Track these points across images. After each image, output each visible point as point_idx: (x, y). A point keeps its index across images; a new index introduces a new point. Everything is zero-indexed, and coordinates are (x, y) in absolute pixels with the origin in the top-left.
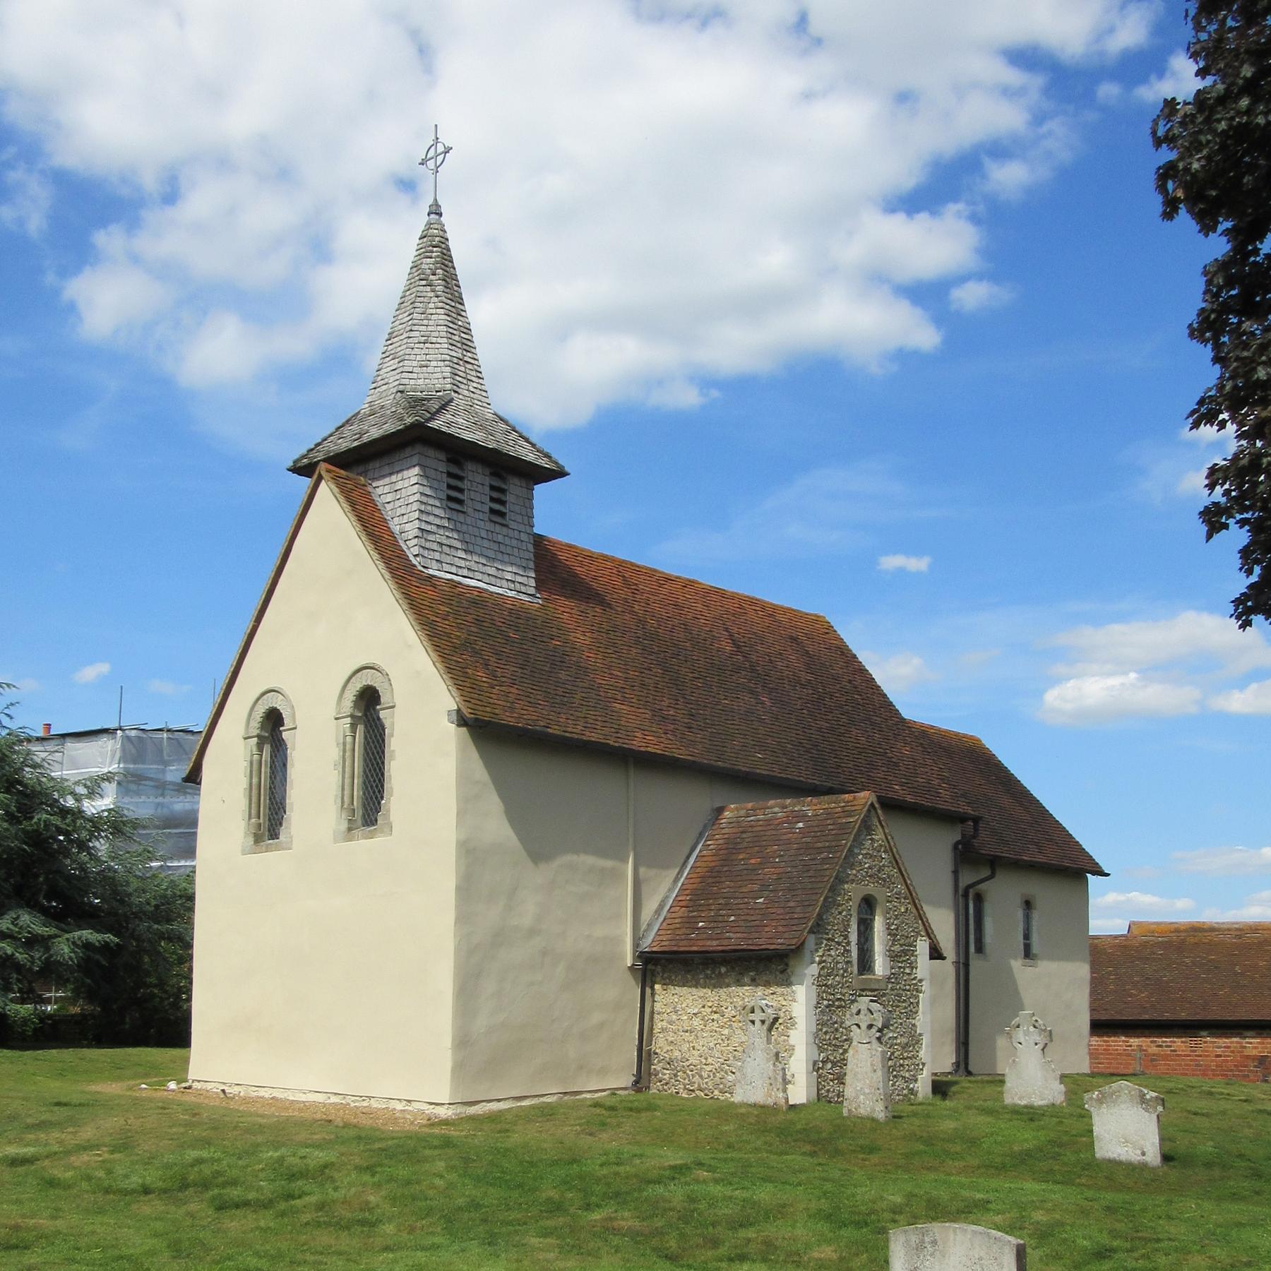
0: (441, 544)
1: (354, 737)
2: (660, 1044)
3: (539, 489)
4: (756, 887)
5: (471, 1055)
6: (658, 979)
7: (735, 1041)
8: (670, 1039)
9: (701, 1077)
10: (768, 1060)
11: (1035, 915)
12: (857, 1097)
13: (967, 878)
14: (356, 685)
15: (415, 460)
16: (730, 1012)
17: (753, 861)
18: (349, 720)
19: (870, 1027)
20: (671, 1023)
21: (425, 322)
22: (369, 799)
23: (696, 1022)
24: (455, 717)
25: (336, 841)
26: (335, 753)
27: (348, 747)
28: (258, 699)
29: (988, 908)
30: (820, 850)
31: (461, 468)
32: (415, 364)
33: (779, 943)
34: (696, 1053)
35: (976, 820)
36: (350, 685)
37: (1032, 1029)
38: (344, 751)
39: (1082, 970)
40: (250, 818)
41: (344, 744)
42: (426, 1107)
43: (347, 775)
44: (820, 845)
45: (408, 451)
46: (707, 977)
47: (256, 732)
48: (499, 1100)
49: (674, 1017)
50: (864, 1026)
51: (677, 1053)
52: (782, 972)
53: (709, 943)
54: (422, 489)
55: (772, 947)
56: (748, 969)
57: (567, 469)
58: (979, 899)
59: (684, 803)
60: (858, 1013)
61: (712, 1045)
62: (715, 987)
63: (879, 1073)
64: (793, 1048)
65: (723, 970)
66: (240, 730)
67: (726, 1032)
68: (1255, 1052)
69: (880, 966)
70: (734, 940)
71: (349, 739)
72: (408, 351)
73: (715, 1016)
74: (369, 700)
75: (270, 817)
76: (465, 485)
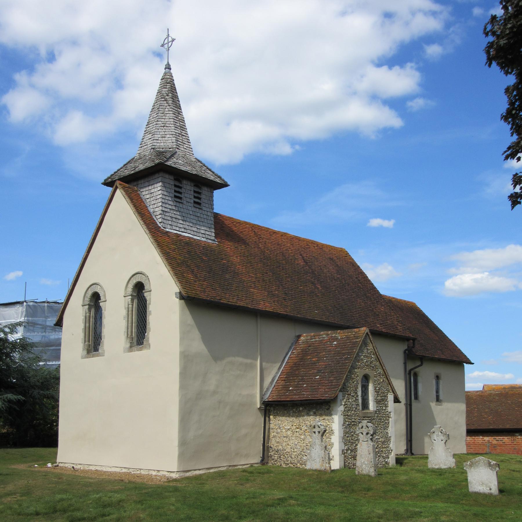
1: (133, 305)
2: (273, 443)
3: (216, 193)
5: (187, 449)
6: (272, 413)
7: (307, 441)
8: (277, 441)
9: (291, 457)
10: (322, 450)
11: (441, 382)
12: (362, 466)
13: (410, 366)
14: (134, 281)
16: (305, 428)
17: (314, 359)
18: (130, 297)
19: (367, 434)
21: (164, 117)
22: (139, 333)
23: (289, 433)
25: (124, 352)
26: (124, 312)
27: (130, 309)
29: (420, 379)
30: (344, 354)
32: (159, 136)
33: (326, 397)
34: (289, 447)
35: (414, 340)
36: (131, 282)
37: (440, 434)
38: (128, 311)
39: (463, 407)
40: (85, 342)
41: (128, 308)
43: (130, 322)
45: (157, 175)
46: (294, 412)
49: (279, 431)
50: (365, 433)
51: (280, 447)
52: (328, 409)
53: (294, 397)
54: (163, 192)
57: (229, 183)
58: (416, 375)
62: (297, 416)
63: (372, 455)
65: (301, 409)
67: (302, 437)
69: (372, 406)
70: (306, 395)
71: (130, 306)
73: (298, 430)
74: (139, 289)
75: (94, 342)
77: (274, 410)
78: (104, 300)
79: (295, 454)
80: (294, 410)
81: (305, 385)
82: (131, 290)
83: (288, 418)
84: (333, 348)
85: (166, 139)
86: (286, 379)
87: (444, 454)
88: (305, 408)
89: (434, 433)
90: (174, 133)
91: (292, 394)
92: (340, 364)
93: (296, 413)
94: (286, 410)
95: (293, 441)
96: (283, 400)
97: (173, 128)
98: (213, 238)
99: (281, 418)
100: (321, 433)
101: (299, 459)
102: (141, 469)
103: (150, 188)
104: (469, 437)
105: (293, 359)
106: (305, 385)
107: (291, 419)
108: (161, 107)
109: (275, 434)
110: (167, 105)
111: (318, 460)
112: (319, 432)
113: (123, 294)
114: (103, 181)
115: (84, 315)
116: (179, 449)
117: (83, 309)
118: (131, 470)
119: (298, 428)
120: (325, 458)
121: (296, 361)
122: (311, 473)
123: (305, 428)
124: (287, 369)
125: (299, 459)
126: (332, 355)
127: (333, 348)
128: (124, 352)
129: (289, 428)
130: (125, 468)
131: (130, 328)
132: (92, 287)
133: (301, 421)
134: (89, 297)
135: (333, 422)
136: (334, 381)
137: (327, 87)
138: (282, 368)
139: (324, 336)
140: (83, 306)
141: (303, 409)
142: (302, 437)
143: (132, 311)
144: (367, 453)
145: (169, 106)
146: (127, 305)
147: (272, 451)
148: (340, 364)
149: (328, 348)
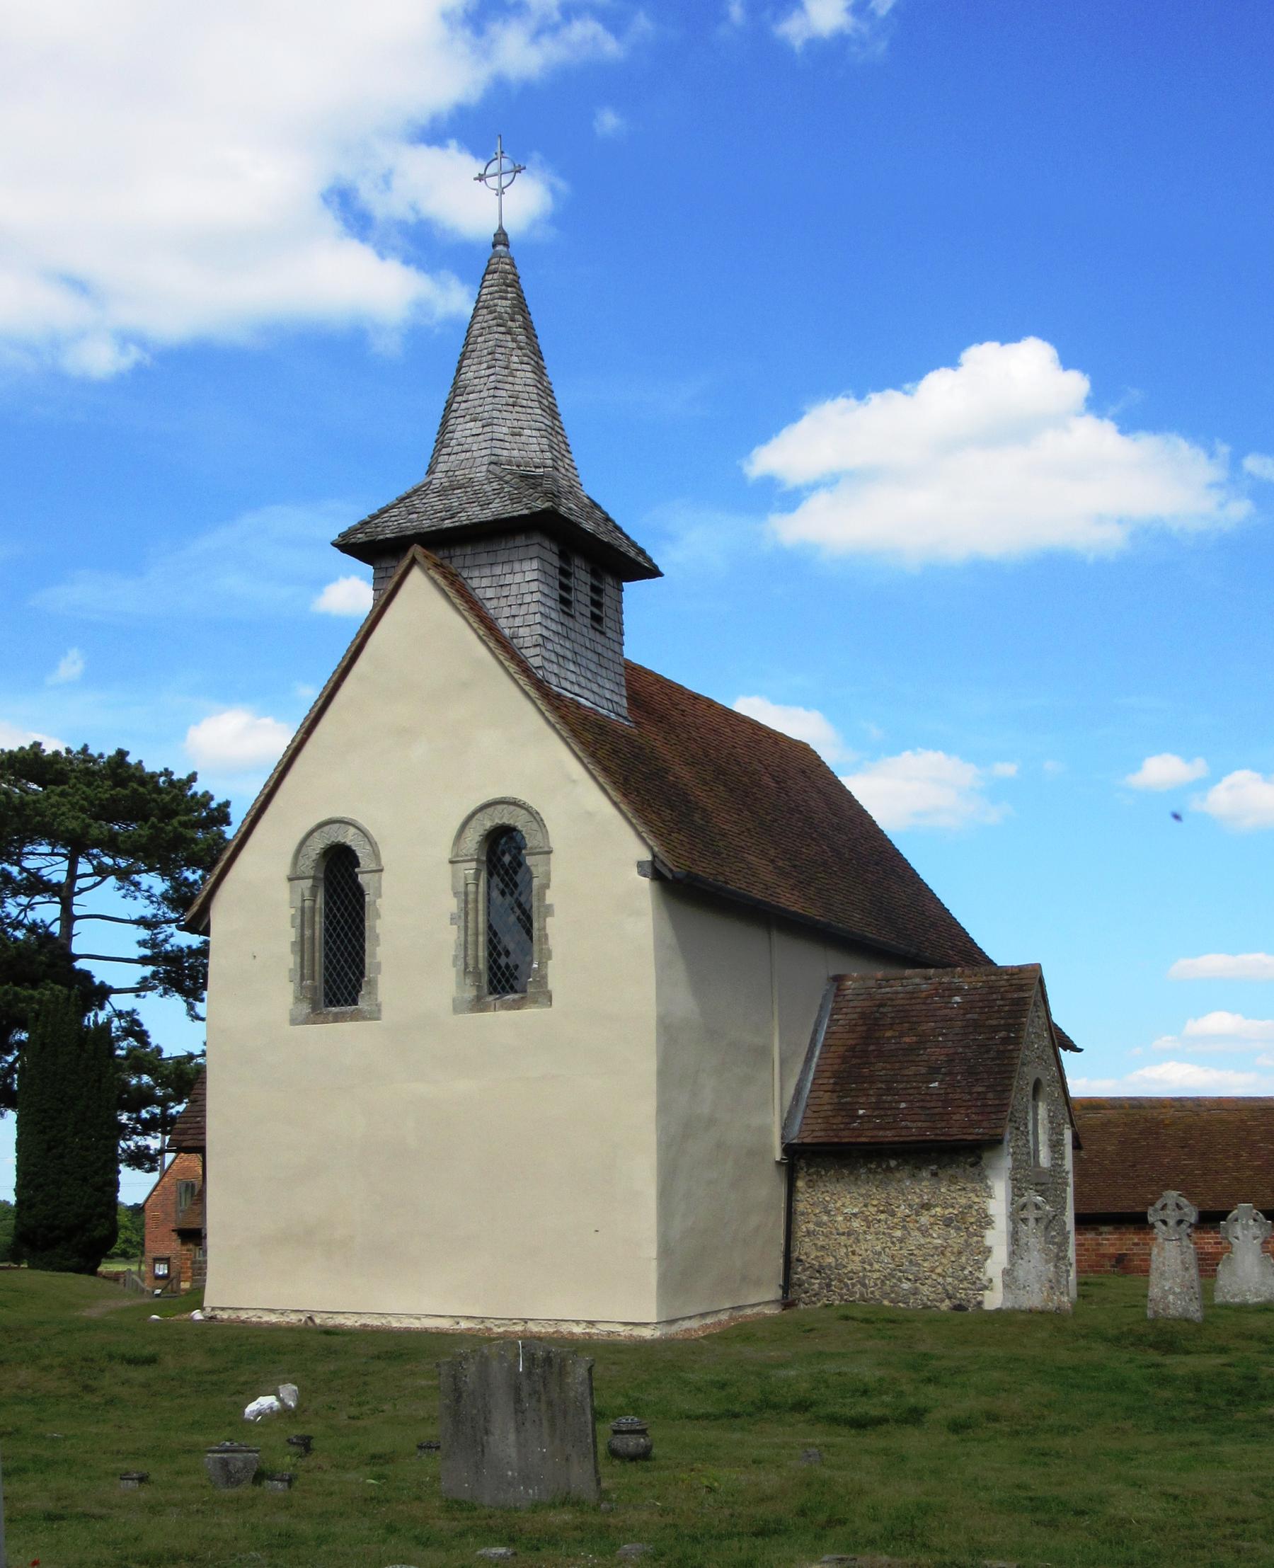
0: (557, 654)
1: (477, 885)
2: (806, 1249)
3: (632, 590)
4: (923, 1070)
5: (679, 1268)
6: (802, 1174)
7: (911, 1244)
8: (820, 1243)
9: (864, 1285)
10: (1047, 1262)
12: (1165, 1297)
14: (487, 822)
15: (534, 550)
17: (907, 1040)
18: (474, 865)
19: (1180, 1222)
20: (819, 1224)
21: (510, 379)
22: (505, 965)
23: (856, 1224)
24: (649, 870)
25: (457, 1009)
26: (452, 905)
27: (471, 897)
30: (996, 1029)
31: (569, 564)
32: (505, 430)
33: (977, 1133)
34: (857, 1258)
36: (473, 823)
37: (1251, 1222)
38: (466, 902)
40: (302, 978)
41: (466, 894)
42: (620, 1328)
43: (470, 932)
44: (994, 1022)
45: (520, 540)
46: (870, 1170)
47: (312, 873)
48: (690, 1318)
49: (825, 1218)
50: (1171, 1222)
51: (831, 1260)
52: (972, 1165)
53: (881, 1133)
54: (542, 587)
55: (970, 1138)
56: (928, 1162)
57: (661, 569)
59: (810, 969)
60: (1164, 1207)
61: (878, 1248)
63: (1193, 1271)
64: (988, 1251)
65: (893, 1163)
66: (283, 867)
67: (898, 1233)
68: (1112, 1250)
70: (915, 1129)
71: (471, 888)
72: (495, 414)
73: (882, 1216)
76: (572, 582)
77: (809, 1166)
78: (373, 866)
79: (876, 1275)
80: (873, 1166)
81: (903, 1105)
82: (475, 846)
83: (854, 1189)
84: (955, 1012)
85: (523, 439)
86: (838, 1088)
87: (1256, 1270)
88: (906, 1162)
89: (1236, 1220)
90: (544, 427)
91: (871, 1125)
92: (992, 1054)
94: (845, 1166)
96: (846, 1140)
97: (539, 411)
98: (624, 713)
99: (830, 1187)
100: (1045, 1222)
101: (887, 1288)
102: (525, 1321)
103: (498, 570)
104: (1090, 1236)
105: (838, 1036)
106: (903, 1105)
108: (500, 350)
109: (811, 1226)
110: (514, 345)
111: (1036, 1287)
112: (1037, 1220)
114: (335, 537)
115: (299, 904)
116: (659, 1265)
117: (292, 891)
118: (488, 1324)
119: (882, 1212)
120: (1058, 1282)
121: (853, 1042)
122: (1022, 1317)
123: (903, 1210)
124: (829, 1061)
126: (957, 1030)
127: (955, 1012)
128: (457, 1009)
129: (856, 1210)
130: (468, 1318)
131: (471, 947)
132: (326, 829)
133: (893, 1194)
134: (314, 857)
135: (990, 1197)
136: (990, 1095)
137: (271, 180)
138: (815, 1060)
139: (917, 980)
140: (290, 880)
141: (898, 1165)
142: (898, 1233)
143: (476, 901)
144: (1180, 1267)
145: (521, 349)
146: (462, 883)
147: (804, 1270)
148: (992, 1054)
149: (938, 1013)
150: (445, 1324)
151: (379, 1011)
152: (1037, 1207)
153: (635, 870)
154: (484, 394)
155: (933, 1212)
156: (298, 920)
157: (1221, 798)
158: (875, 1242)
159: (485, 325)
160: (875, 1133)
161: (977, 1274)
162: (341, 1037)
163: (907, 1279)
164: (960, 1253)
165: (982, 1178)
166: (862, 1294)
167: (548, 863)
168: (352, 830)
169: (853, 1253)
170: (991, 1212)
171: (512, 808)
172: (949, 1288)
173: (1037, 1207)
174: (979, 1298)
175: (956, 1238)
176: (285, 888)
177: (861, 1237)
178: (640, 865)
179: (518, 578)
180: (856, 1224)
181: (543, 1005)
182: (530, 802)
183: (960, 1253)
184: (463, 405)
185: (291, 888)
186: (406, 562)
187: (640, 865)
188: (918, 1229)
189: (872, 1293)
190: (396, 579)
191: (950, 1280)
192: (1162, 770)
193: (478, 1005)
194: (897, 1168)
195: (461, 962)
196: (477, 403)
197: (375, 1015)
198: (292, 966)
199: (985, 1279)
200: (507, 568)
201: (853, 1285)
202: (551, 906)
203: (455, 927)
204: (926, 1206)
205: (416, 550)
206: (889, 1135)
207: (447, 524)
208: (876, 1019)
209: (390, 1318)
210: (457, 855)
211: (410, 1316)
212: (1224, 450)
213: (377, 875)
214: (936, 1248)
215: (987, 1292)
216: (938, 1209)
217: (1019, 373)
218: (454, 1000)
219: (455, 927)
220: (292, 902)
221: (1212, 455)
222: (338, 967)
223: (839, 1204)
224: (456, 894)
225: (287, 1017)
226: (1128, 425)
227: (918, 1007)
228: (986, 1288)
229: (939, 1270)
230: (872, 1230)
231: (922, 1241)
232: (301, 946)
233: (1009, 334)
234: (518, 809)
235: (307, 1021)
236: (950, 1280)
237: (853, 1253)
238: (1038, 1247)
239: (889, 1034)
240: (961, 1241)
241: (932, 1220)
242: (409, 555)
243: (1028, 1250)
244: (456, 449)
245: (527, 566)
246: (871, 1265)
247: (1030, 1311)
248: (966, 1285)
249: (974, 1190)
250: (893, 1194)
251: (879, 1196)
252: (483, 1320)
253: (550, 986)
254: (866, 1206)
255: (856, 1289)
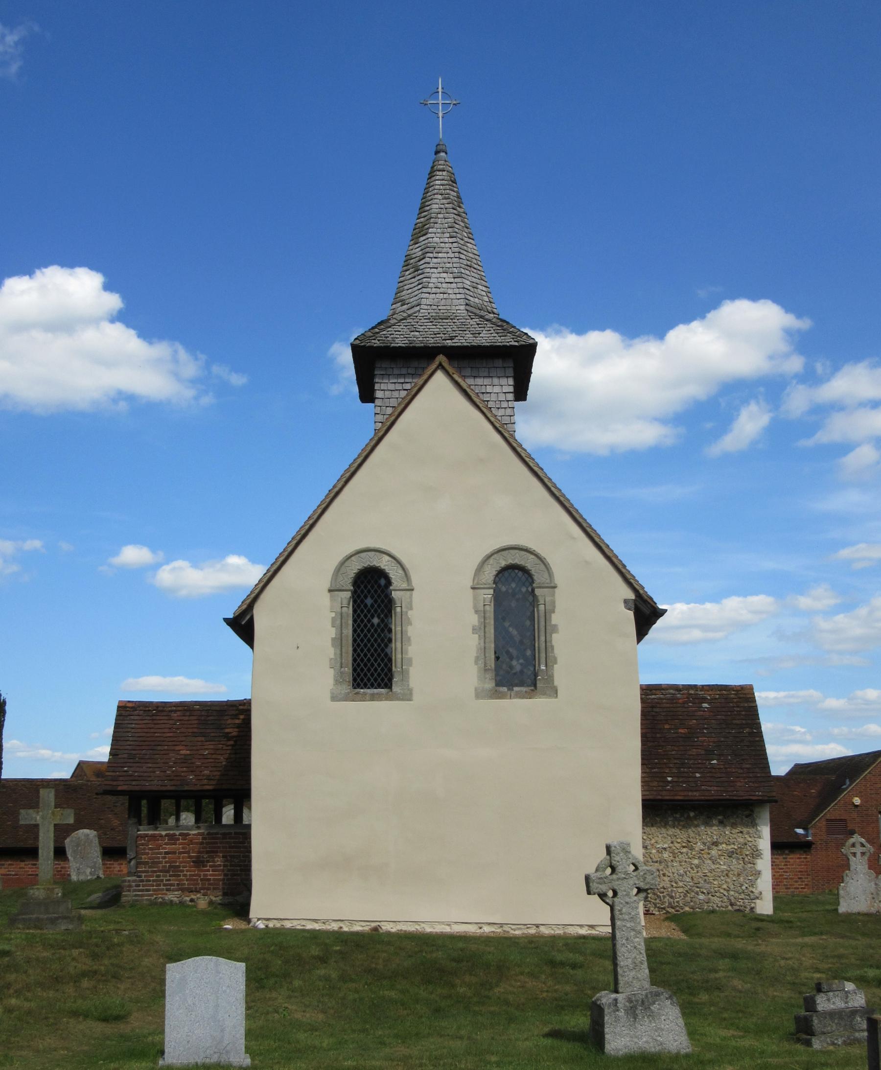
4: (703, 752)
10: (870, 881)
17: (682, 731)
23: (666, 855)
26: (474, 619)
28: (492, 554)
34: (666, 878)
36: (491, 561)
41: (484, 612)
45: (499, 363)
46: (675, 819)
52: (747, 817)
53: (690, 794)
62: (684, 827)
64: (759, 873)
65: (692, 814)
67: (696, 862)
70: (713, 791)
73: (685, 850)
78: (404, 586)
79: (680, 890)
80: (678, 816)
83: (663, 830)
84: (707, 713)
93: (679, 821)
95: (676, 868)
102: (537, 926)
107: (671, 831)
112: (863, 854)
113: (470, 584)
115: (339, 610)
118: (506, 928)
119: (684, 847)
123: (699, 846)
125: (688, 899)
129: (666, 846)
130: (489, 924)
135: (760, 837)
140: (330, 591)
142: (696, 862)
149: (696, 714)
150: (472, 929)
151: (411, 694)
152: (863, 845)
153: (622, 605)
154: (452, 255)
155: (720, 847)
156: (338, 622)
157: (166, 576)
158: (679, 868)
159: (442, 206)
160: (686, 793)
161: (751, 889)
162: (374, 711)
163: (703, 893)
164: (739, 875)
165: (754, 824)
166: (670, 903)
167: (553, 595)
168: (387, 558)
169: (664, 875)
170: (760, 847)
171: (523, 553)
172: (732, 898)
173: (863, 845)
174: (753, 905)
175: (736, 865)
176: (325, 599)
177: (670, 864)
178: (626, 602)
179: (497, 389)
180: (666, 855)
181: (550, 696)
182: (539, 551)
183: (739, 875)
184: (435, 260)
185: (331, 597)
186: (434, 366)
187: (626, 602)
188: (710, 859)
189: (678, 902)
190: (425, 377)
191: (732, 893)
192: (133, 555)
193: (495, 695)
194: (695, 818)
195: (481, 662)
196: (446, 260)
197: (407, 696)
198: (332, 656)
199: (756, 892)
200: (487, 381)
201: (664, 897)
202: (556, 626)
203: (477, 636)
204: (716, 844)
205: (441, 358)
206: (696, 795)
207: (449, 343)
208: (653, 716)
209: (423, 925)
210: (478, 584)
211: (443, 923)
212: (203, 357)
213: (408, 593)
214: (723, 872)
215: (757, 901)
216: (724, 845)
217: (79, 288)
218: (476, 689)
219: (477, 636)
220: (332, 607)
221: (196, 359)
222: (372, 658)
223: (653, 841)
224: (476, 612)
225: (329, 695)
226: (146, 334)
227: (679, 709)
228: (757, 898)
229: (725, 886)
230: (677, 859)
231: (713, 867)
232: (338, 641)
233: (69, 262)
234: (528, 554)
235: (346, 699)
236: (732, 893)
237: (664, 875)
238: (864, 871)
239: (667, 726)
240: (740, 866)
241: (720, 853)
242: (437, 362)
243: (856, 873)
244: (434, 290)
245: (504, 381)
246: (676, 883)
247: (859, 913)
248: (743, 896)
249: (748, 833)
250: (692, 835)
251: (681, 835)
252: (501, 925)
253: (556, 683)
254: (672, 843)
255: (666, 900)
